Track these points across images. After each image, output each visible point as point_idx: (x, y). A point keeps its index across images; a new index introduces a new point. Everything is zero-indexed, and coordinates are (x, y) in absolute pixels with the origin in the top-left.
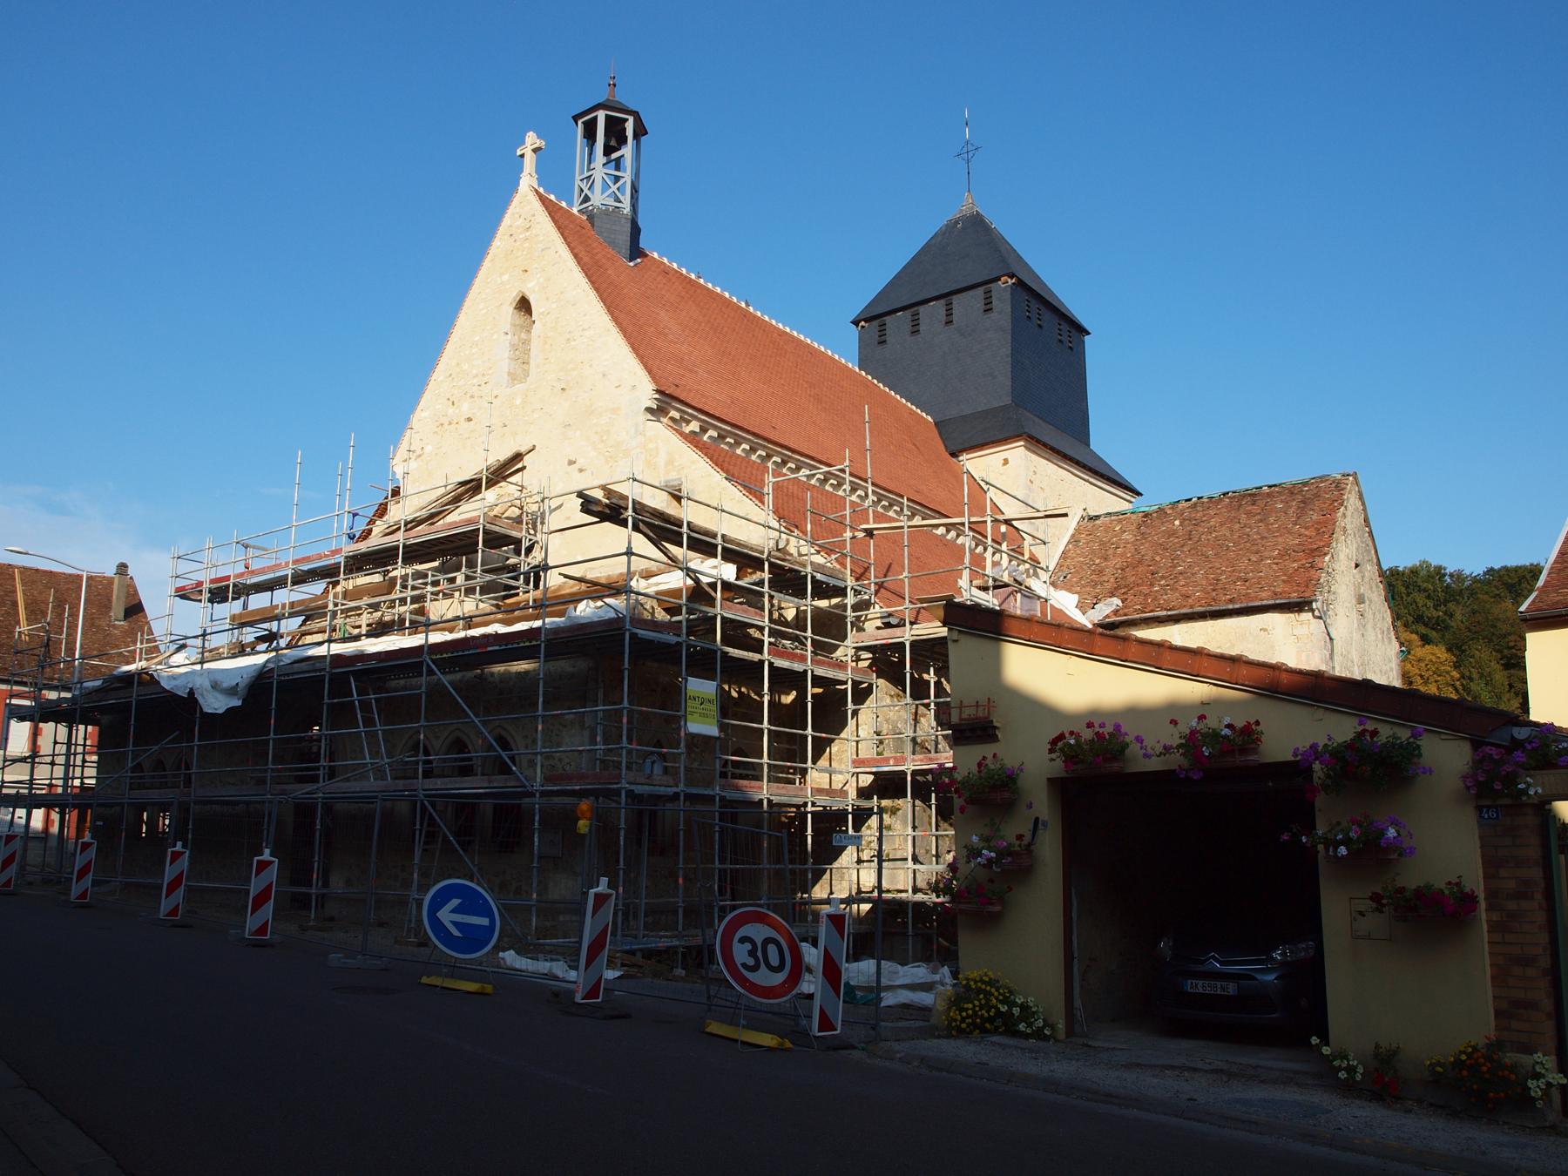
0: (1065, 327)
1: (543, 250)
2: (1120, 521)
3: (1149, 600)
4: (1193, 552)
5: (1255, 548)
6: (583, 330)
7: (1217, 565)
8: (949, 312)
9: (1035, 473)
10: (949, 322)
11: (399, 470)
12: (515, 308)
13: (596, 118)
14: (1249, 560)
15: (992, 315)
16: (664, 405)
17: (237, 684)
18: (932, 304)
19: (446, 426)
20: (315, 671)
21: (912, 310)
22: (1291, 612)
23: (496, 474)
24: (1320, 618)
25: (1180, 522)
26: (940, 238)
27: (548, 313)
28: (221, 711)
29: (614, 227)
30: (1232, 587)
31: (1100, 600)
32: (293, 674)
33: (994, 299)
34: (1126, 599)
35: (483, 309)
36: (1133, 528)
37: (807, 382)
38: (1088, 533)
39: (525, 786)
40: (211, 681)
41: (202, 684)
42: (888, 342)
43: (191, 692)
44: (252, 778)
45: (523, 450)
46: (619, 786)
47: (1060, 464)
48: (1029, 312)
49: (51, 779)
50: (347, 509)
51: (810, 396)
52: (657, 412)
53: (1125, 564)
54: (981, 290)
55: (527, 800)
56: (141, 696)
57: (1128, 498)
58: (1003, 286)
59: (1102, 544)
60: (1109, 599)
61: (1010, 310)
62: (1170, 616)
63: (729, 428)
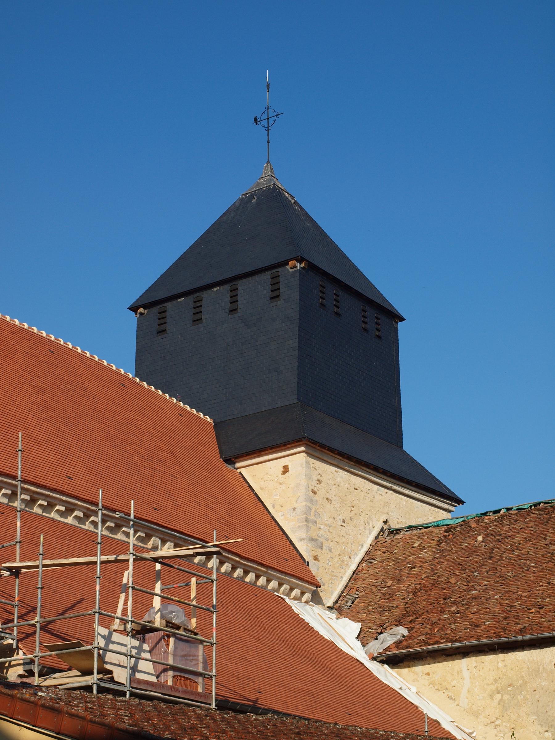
0: (371, 313)
2: (420, 536)
3: (436, 630)
4: (491, 573)
7: (515, 589)
8: (234, 300)
9: (319, 482)
10: (233, 311)
14: (549, 583)
15: (279, 303)
18: (215, 289)
25: (484, 538)
31: (385, 629)
33: (281, 286)
34: (412, 628)
36: (433, 544)
37: (34, 387)
38: (385, 549)
42: (168, 331)
47: (351, 470)
48: (323, 299)
51: (33, 403)
53: (418, 586)
54: (267, 276)
57: (446, 506)
58: (291, 270)
59: (398, 562)
60: (395, 628)
61: (298, 297)
62: (457, 648)
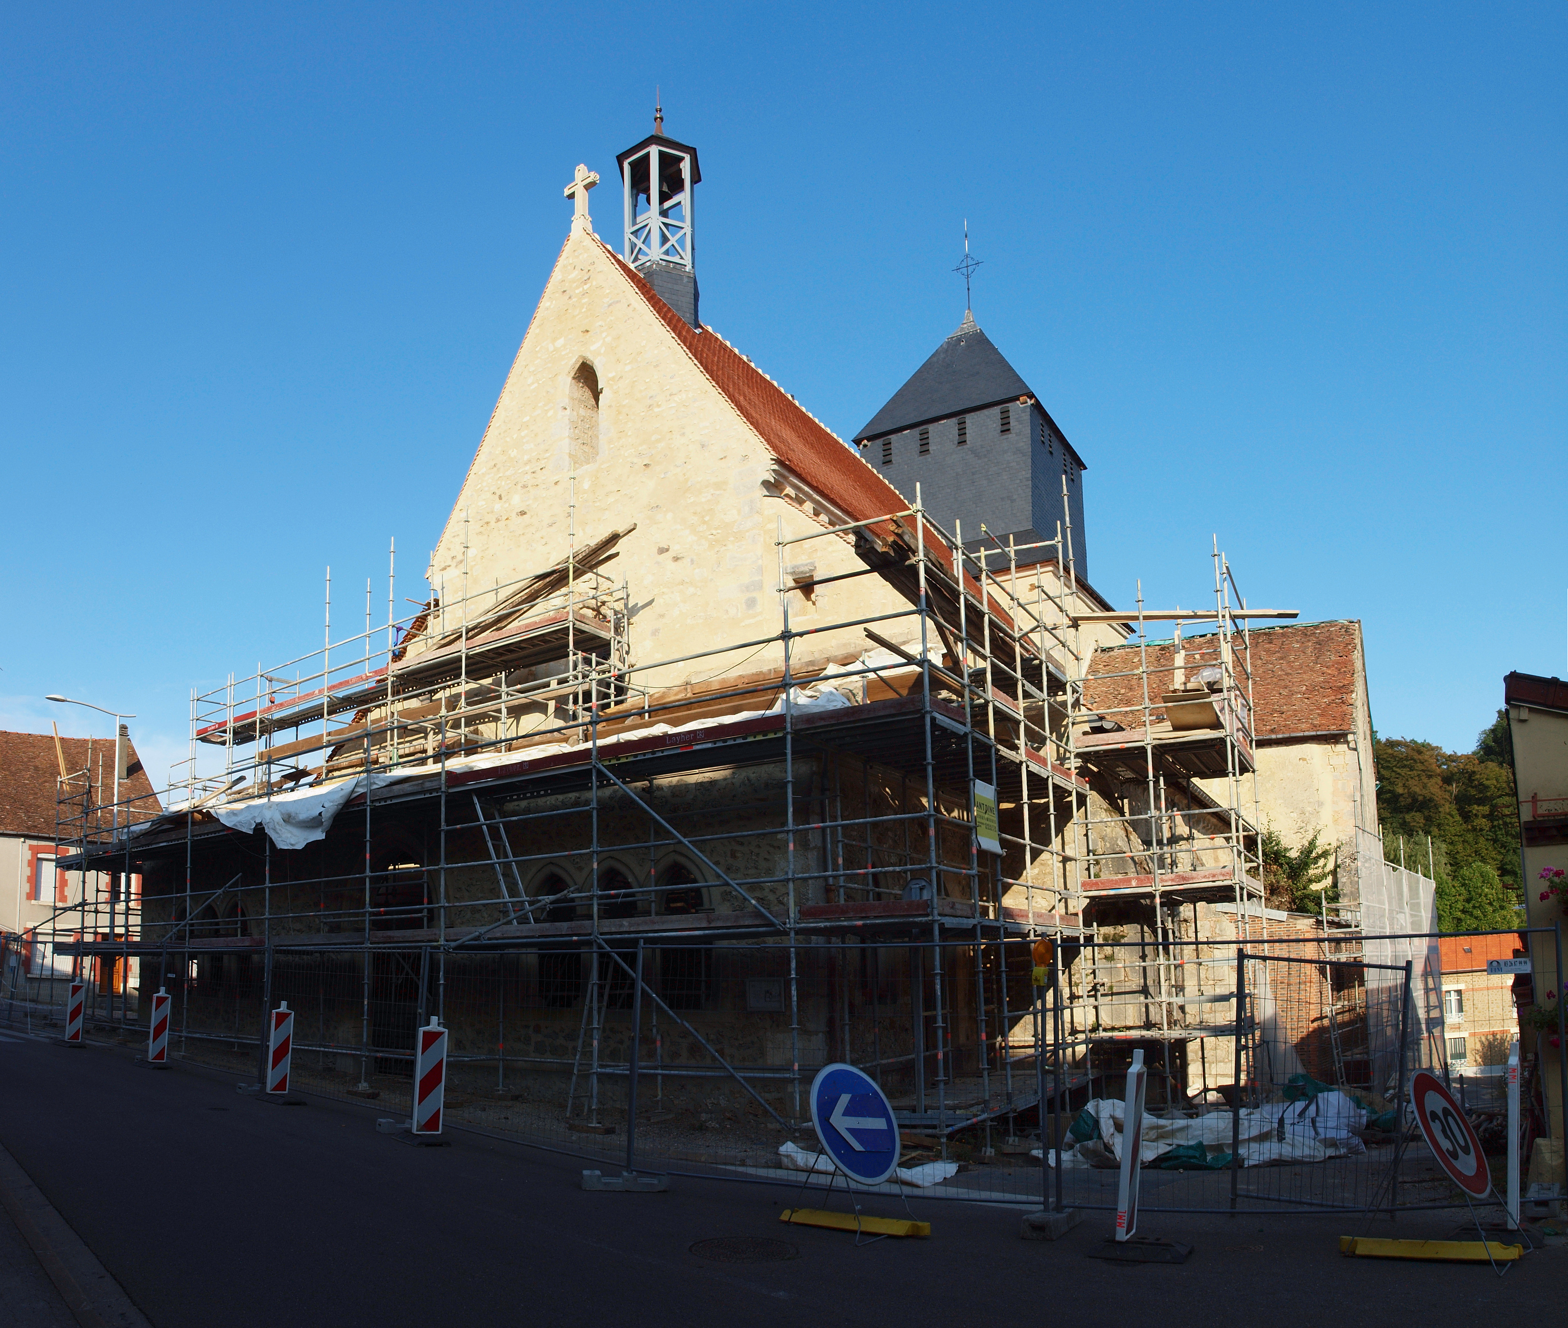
1: (610, 305)
5: (1282, 683)
6: (671, 395)
8: (962, 432)
11: (436, 583)
12: (574, 378)
13: (648, 155)
15: (1010, 436)
16: (781, 480)
17: (320, 814)
18: (942, 422)
19: (493, 524)
20: (424, 792)
21: (921, 428)
22: (1328, 744)
23: (583, 563)
24: (1355, 749)
26: (942, 356)
27: (621, 377)
28: (300, 846)
29: (676, 287)
30: (1270, 718)
32: (391, 798)
35: (533, 383)
39: (772, 924)
40: (282, 814)
41: (270, 817)
42: (894, 462)
43: (260, 829)
44: (325, 923)
45: (621, 530)
46: (930, 918)
49: (96, 927)
50: (391, 622)
52: (773, 488)
54: (997, 410)
55: (584, 950)
56: (197, 836)
57: (1125, 634)
63: (840, 514)
